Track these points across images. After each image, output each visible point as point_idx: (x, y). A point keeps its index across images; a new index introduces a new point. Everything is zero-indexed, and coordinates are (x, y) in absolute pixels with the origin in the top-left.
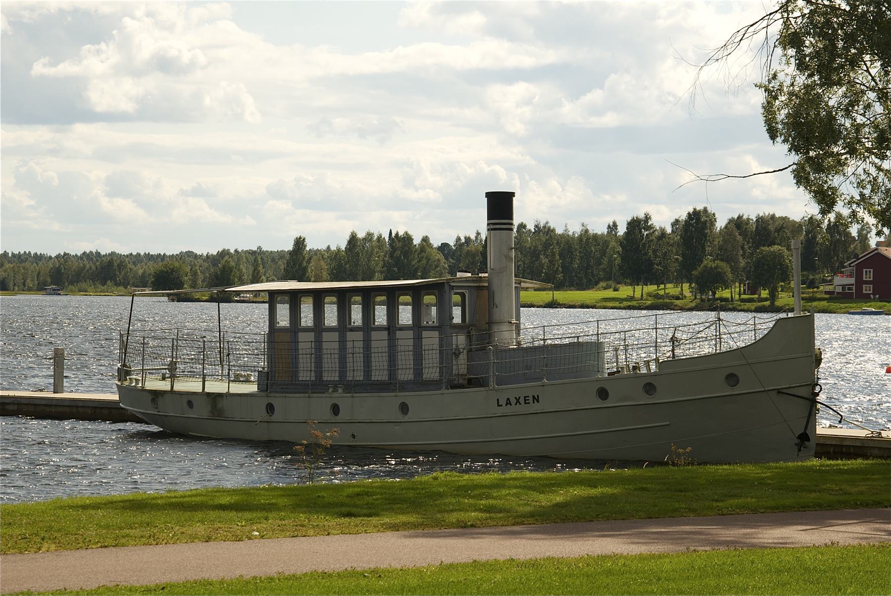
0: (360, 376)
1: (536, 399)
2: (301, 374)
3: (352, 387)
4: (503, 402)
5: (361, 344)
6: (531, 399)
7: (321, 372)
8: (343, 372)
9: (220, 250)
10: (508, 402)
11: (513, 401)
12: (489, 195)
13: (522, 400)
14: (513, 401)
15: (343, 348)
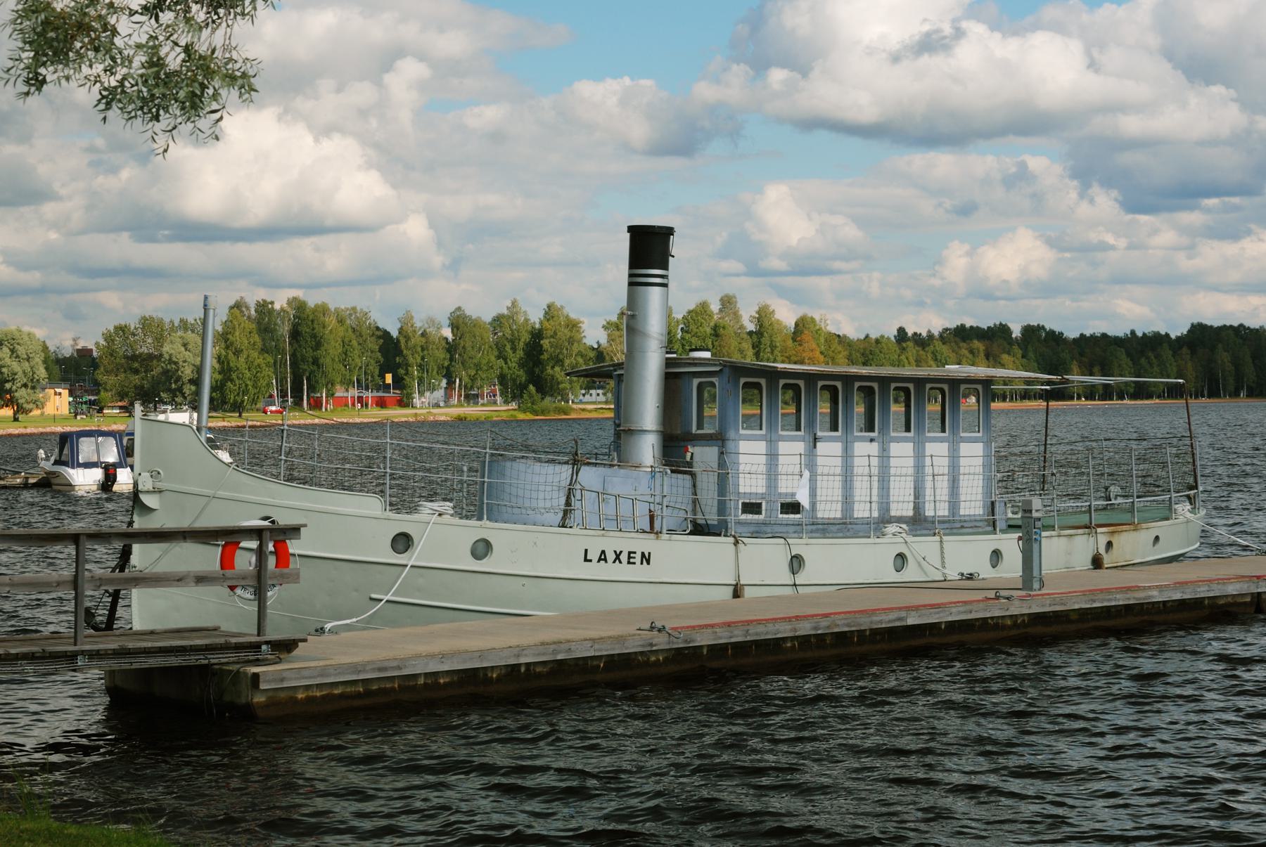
0: (943, 511)
1: (646, 558)
2: (856, 506)
3: (918, 522)
4: (593, 555)
5: (946, 461)
6: (638, 556)
7: (888, 503)
8: (954, 504)
9: (874, 335)
10: (603, 557)
11: (611, 556)
12: (632, 230)
13: (624, 557)
14: (611, 556)
15: (919, 468)
